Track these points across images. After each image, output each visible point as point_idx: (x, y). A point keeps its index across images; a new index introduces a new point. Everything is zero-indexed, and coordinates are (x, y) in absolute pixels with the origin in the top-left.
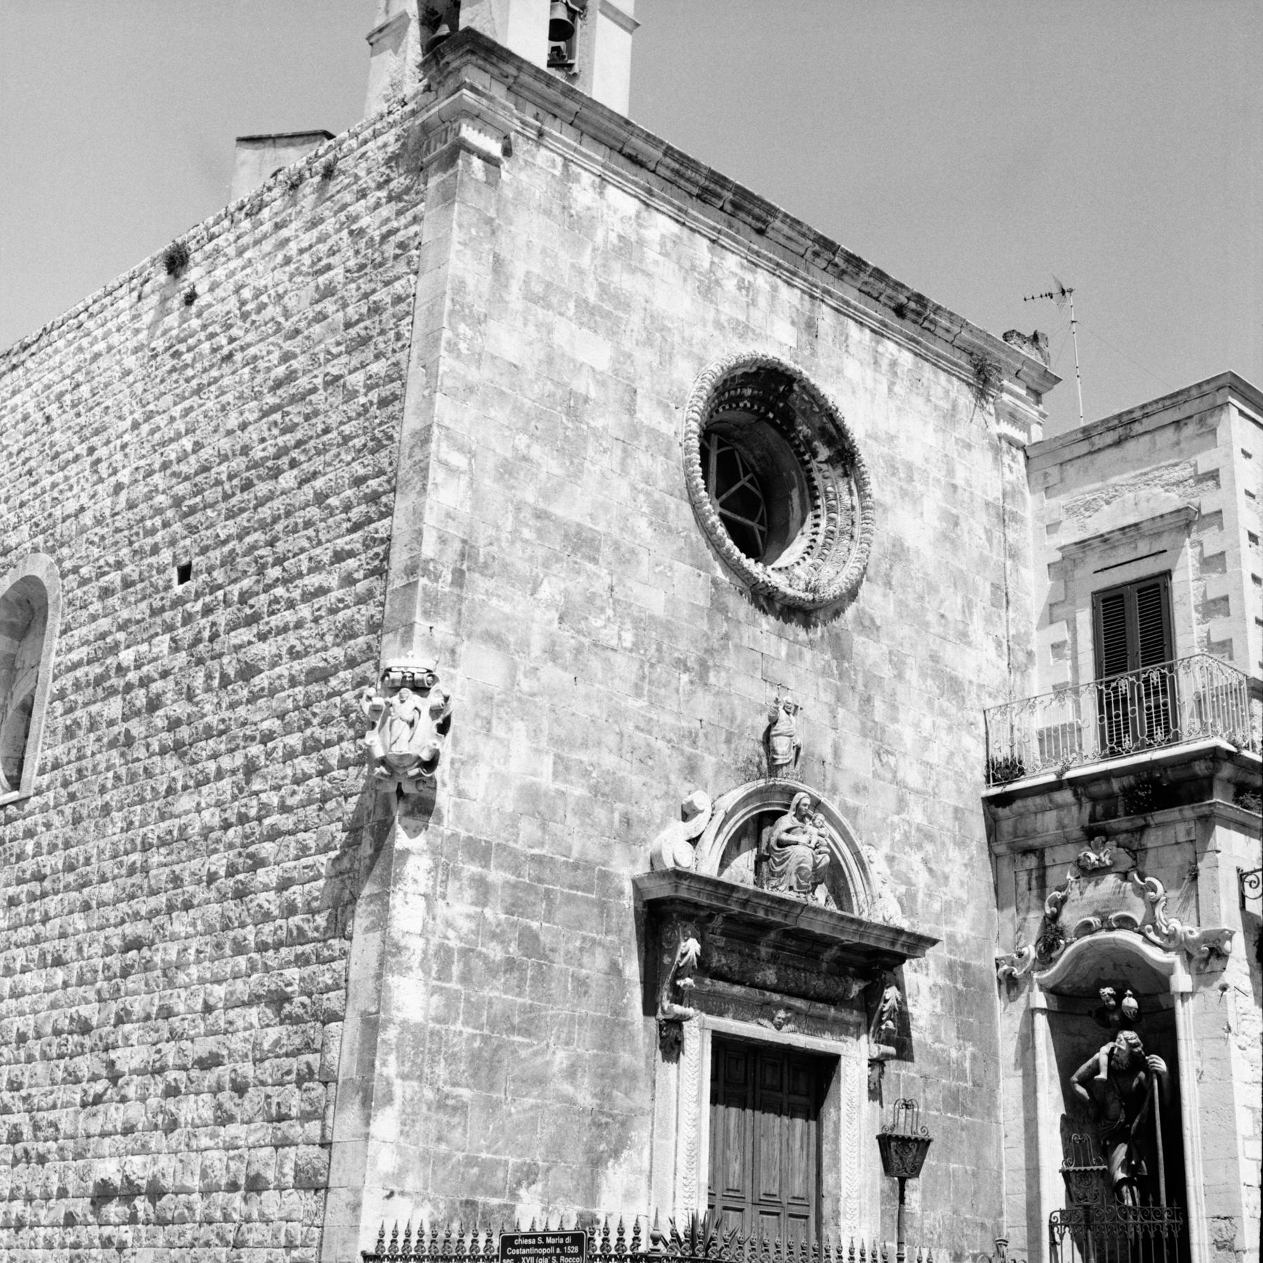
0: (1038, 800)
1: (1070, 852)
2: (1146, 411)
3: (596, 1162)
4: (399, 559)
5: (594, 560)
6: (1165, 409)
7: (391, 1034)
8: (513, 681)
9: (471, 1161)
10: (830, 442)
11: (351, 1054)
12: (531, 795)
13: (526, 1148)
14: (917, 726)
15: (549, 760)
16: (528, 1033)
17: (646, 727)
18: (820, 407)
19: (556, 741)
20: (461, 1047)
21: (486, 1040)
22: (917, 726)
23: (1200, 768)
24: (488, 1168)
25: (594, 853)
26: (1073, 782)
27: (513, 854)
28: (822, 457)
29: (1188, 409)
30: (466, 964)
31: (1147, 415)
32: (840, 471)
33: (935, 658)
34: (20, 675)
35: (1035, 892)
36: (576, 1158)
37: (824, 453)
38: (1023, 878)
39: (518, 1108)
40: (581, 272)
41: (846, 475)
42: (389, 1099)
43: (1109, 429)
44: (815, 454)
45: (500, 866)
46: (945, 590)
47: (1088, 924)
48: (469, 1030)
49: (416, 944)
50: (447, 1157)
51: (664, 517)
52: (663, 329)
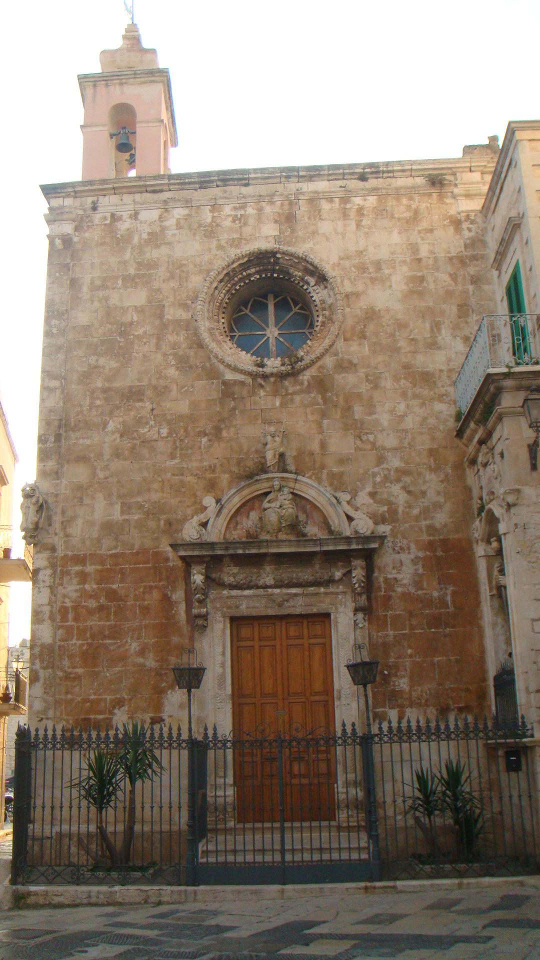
18: (298, 258)
28: (312, 284)
32: (322, 287)
37: (312, 281)
41: (326, 287)
44: (308, 284)
50: (72, 700)
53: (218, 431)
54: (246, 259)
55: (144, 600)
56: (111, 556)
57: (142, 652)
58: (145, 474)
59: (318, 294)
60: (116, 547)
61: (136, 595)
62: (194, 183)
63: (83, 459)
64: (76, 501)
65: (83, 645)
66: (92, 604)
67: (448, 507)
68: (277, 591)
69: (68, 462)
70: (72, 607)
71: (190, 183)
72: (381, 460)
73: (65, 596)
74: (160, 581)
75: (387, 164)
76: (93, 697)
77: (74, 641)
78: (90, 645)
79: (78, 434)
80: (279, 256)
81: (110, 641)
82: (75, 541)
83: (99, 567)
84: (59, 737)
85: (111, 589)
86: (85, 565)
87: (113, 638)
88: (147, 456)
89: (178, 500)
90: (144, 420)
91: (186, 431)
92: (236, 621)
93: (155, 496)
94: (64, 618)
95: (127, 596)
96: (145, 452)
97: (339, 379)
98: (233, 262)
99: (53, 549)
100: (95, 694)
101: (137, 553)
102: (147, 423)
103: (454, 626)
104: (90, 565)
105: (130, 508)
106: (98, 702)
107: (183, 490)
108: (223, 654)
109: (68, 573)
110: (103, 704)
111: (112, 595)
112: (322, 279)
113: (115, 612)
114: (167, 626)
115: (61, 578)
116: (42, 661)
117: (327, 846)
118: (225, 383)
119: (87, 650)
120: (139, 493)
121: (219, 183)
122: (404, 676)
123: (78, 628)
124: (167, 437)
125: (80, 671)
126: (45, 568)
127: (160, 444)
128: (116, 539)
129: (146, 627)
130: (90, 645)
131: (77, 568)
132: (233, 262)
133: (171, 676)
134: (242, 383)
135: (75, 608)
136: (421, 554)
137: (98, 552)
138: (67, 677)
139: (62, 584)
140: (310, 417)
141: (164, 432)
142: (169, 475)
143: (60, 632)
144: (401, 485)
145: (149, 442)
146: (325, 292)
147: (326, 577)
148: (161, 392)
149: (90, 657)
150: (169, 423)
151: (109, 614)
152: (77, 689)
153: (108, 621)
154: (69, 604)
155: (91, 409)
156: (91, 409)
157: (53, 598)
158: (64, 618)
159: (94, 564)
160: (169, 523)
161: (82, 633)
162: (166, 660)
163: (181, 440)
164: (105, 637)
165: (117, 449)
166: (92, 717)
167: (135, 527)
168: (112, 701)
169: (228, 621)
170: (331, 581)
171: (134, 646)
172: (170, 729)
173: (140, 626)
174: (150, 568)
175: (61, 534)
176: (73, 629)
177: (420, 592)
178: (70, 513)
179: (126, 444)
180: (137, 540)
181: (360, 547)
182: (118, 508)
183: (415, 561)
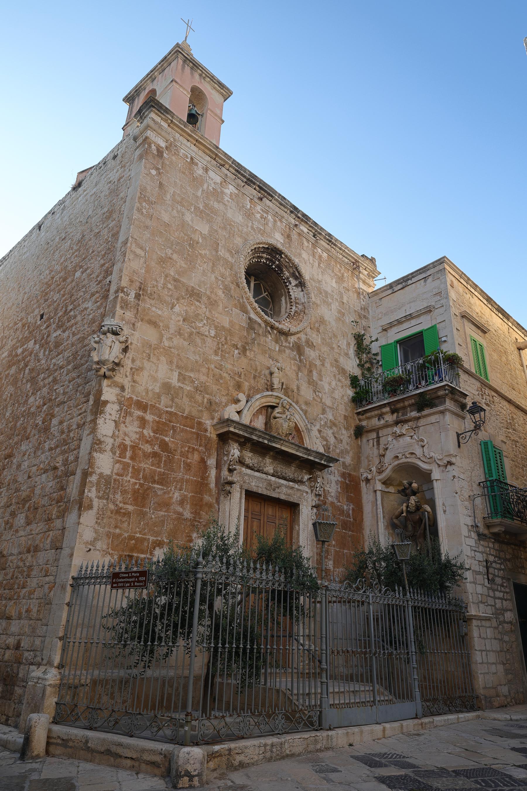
6: (420, 273)
7: (94, 478)
10: (296, 278)
18: (293, 264)
22: (330, 384)
28: (293, 284)
31: (413, 277)
32: (300, 289)
35: (375, 447)
37: (294, 282)
41: (303, 291)
43: (399, 284)
44: (290, 283)
47: (397, 457)
50: (120, 535)
53: (244, 350)
54: (267, 246)
55: (187, 458)
56: (167, 412)
57: (182, 503)
58: (197, 357)
59: (295, 292)
60: (171, 407)
61: (182, 452)
62: (245, 177)
63: (153, 323)
64: (145, 355)
65: (136, 484)
66: (148, 448)
67: (351, 454)
68: (273, 479)
69: (142, 320)
70: (131, 446)
71: (242, 175)
72: (324, 412)
73: (125, 434)
74: (200, 446)
75: (337, 240)
76: (138, 535)
77: (128, 478)
78: (141, 485)
79: (153, 302)
80: (283, 256)
81: (158, 486)
82: (140, 389)
83: (157, 419)
85: (164, 440)
86: (145, 412)
87: (161, 484)
88: (200, 345)
89: (218, 387)
90: (200, 317)
91: (226, 339)
92: (251, 496)
93: (203, 378)
94: (122, 455)
95: (175, 450)
96: (198, 340)
97: (307, 350)
98: (261, 243)
99: (123, 388)
100: (140, 532)
101: (187, 418)
102: (202, 320)
103: (352, 531)
104: (150, 414)
105: (184, 379)
106: (142, 540)
107: (221, 381)
108: (239, 519)
109: (131, 414)
110: (146, 544)
111: (164, 446)
112: (302, 285)
113: (165, 461)
114: (201, 486)
115: (125, 417)
116: (98, 491)
117: (341, 695)
118: (250, 318)
119: (138, 489)
120: (192, 370)
121: (257, 188)
122: (330, 560)
124: (214, 338)
125: (130, 508)
126: (113, 403)
127: (209, 340)
128: (172, 400)
129: (187, 481)
130: (141, 485)
131: (140, 413)
132: (261, 243)
134: (260, 325)
135: (133, 447)
136: (340, 479)
137: (157, 405)
138: (118, 511)
139: (124, 423)
140: (293, 367)
141: (213, 333)
142: (212, 366)
143: (117, 465)
144: (331, 431)
145: (202, 335)
147: (300, 479)
148: (212, 304)
149: (141, 497)
150: (216, 328)
151: (160, 461)
152: (125, 525)
153: (158, 467)
154: (128, 442)
155: (164, 288)
156: (164, 288)
157: (117, 433)
158: (122, 455)
159: (153, 414)
160: (210, 403)
161: (136, 472)
162: (199, 513)
163: (222, 345)
164: (154, 482)
165: (180, 329)
166: (135, 555)
167: (187, 396)
168: (154, 542)
169: (244, 493)
170: (301, 482)
171: (177, 496)
173: (182, 479)
174: (194, 433)
175: (129, 378)
176: (129, 467)
177: (339, 504)
178: (138, 363)
179: (186, 329)
180: (187, 407)
182: (176, 374)
183: (337, 482)
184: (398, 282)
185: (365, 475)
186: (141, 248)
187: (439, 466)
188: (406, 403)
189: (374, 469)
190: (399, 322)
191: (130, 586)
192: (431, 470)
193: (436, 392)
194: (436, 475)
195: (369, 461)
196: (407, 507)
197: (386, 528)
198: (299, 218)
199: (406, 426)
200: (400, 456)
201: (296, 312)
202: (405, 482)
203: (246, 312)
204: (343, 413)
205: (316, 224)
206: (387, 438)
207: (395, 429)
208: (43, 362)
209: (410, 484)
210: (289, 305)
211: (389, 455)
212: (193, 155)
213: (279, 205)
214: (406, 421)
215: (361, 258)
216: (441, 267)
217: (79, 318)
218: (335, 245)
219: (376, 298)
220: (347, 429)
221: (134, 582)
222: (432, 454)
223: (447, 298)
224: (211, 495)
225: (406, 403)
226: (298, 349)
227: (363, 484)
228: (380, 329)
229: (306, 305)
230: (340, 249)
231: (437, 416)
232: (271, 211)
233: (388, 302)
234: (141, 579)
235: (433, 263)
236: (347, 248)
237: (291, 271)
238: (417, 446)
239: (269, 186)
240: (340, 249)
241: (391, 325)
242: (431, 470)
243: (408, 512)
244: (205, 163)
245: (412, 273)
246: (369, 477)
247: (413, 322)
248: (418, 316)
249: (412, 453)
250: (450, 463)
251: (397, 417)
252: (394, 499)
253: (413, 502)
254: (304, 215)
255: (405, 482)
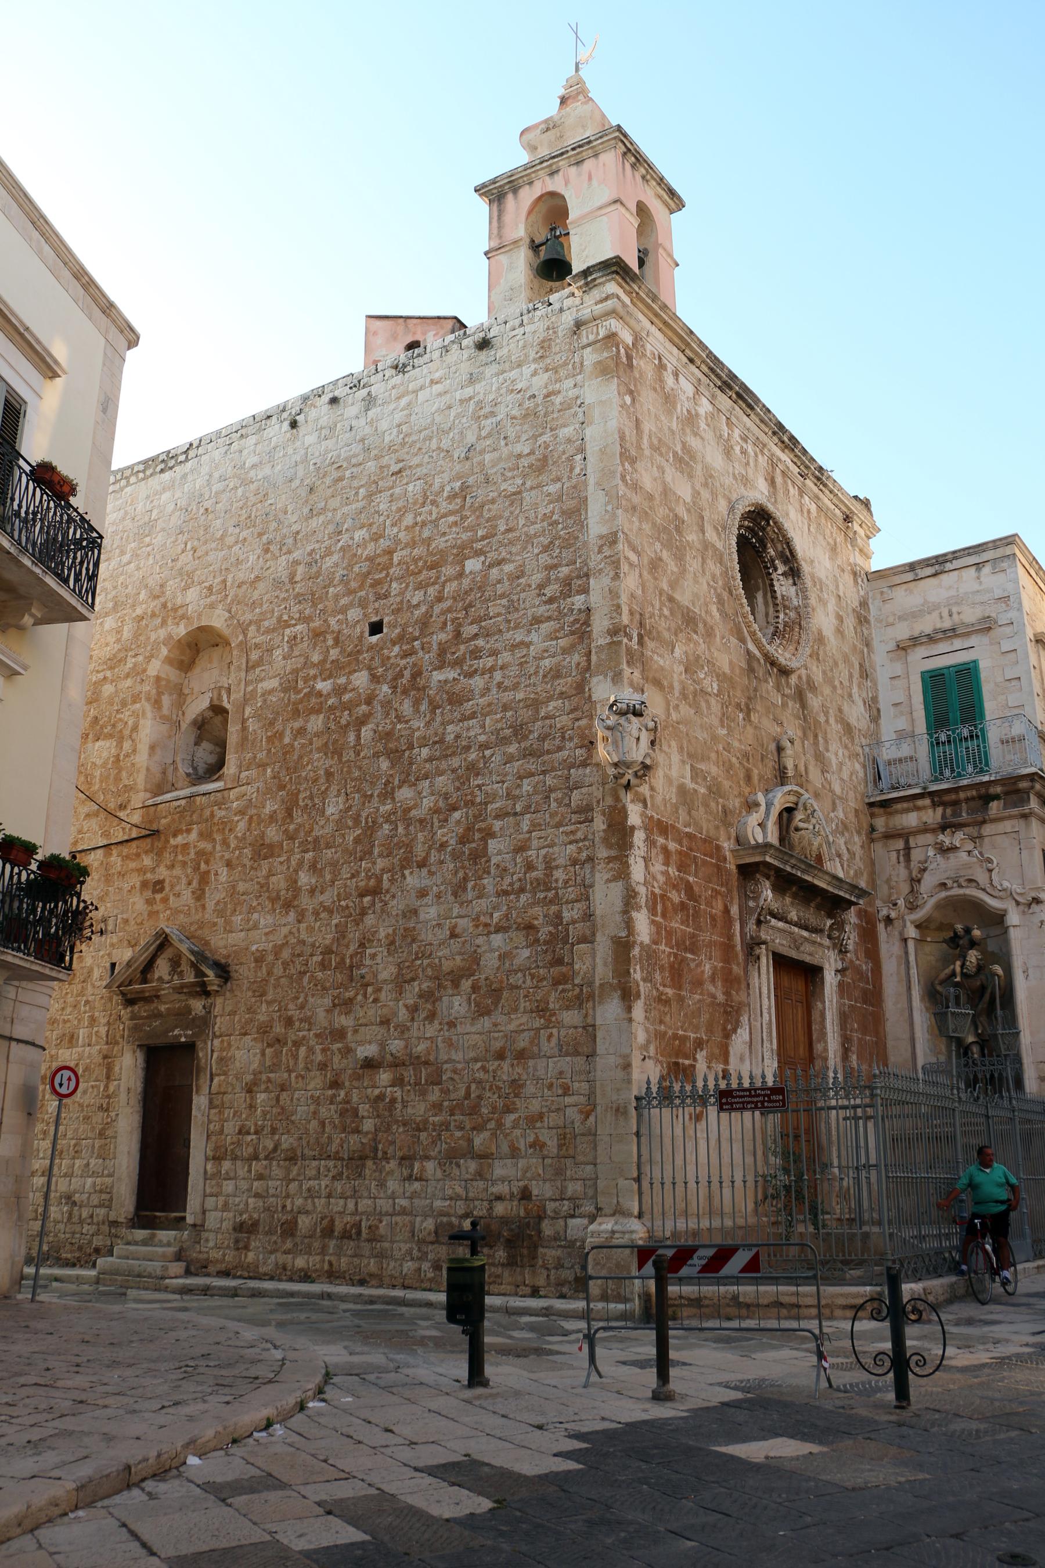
0: (905, 805)
1: (929, 838)
2: (956, 555)
3: (727, 1036)
4: (600, 624)
5: (696, 632)
6: (969, 555)
7: (636, 951)
8: (669, 715)
9: (675, 1036)
10: (786, 561)
11: (605, 964)
12: (682, 790)
13: (696, 1029)
14: (836, 755)
15: (688, 767)
16: (693, 953)
17: (728, 748)
18: (784, 536)
19: (690, 756)
20: (665, 961)
21: (676, 955)
22: (836, 755)
23: (1024, 785)
24: (684, 1039)
25: (712, 833)
26: (931, 794)
27: (678, 830)
28: (780, 572)
29: (985, 556)
30: (664, 904)
31: (956, 558)
32: (791, 581)
33: (840, 710)
34: (189, 700)
35: (902, 864)
36: (718, 1037)
37: (781, 568)
38: (894, 855)
39: (693, 999)
40: (673, 432)
41: (795, 584)
42: (638, 996)
43: (928, 566)
44: (776, 569)
45: (673, 840)
46: (841, 666)
47: (945, 884)
48: (668, 949)
49: (642, 890)
50: (665, 1033)
51: (723, 605)
52: (711, 476)
68: (796, 929)
84: (654, 1089)
112: (794, 573)
123: (588, 1299)
133: (374, 619)
146: (793, 589)
172: (705, 1080)
181: (776, 863)
184: (927, 562)
185: (884, 912)
186: (634, 549)
187: (1018, 903)
188: (962, 795)
189: (901, 902)
190: (931, 639)
191: (756, 1107)
192: (1006, 910)
193: (1015, 783)
194: (1013, 918)
195: (890, 888)
196: (962, 966)
197: (922, 1000)
198: (783, 442)
199: (960, 835)
200: (949, 883)
201: (786, 625)
202: (959, 927)
203: (743, 640)
204: (852, 804)
205: (805, 452)
206: (923, 848)
207: (941, 837)
208: (418, 723)
209: (968, 931)
210: (771, 610)
211: (929, 881)
212: (662, 350)
213: (758, 422)
214: (959, 826)
215: (854, 501)
216: (1008, 551)
217: (505, 657)
218: (825, 485)
219: (882, 584)
220: (859, 833)
221: (762, 1102)
222: (1006, 884)
223: (1020, 609)
224: (738, 964)
225: (962, 795)
226: (800, 696)
227: (881, 927)
228: (892, 646)
229: (802, 611)
230: (831, 492)
231: (1015, 822)
232: (750, 435)
233: (905, 599)
234: (774, 1097)
235: (994, 541)
236: (841, 489)
237: (780, 549)
238: (979, 870)
239: (751, 392)
240: (831, 492)
241: (915, 641)
242: (1006, 910)
243: (964, 975)
244: (675, 363)
245: (954, 552)
246: (893, 915)
247: (958, 644)
248: (967, 635)
249: (970, 881)
250: (1037, 901)
251: (943, 816)
252: (933, 951)
253: (974, 960)
254: (792, 438)
255: (959, 927)
